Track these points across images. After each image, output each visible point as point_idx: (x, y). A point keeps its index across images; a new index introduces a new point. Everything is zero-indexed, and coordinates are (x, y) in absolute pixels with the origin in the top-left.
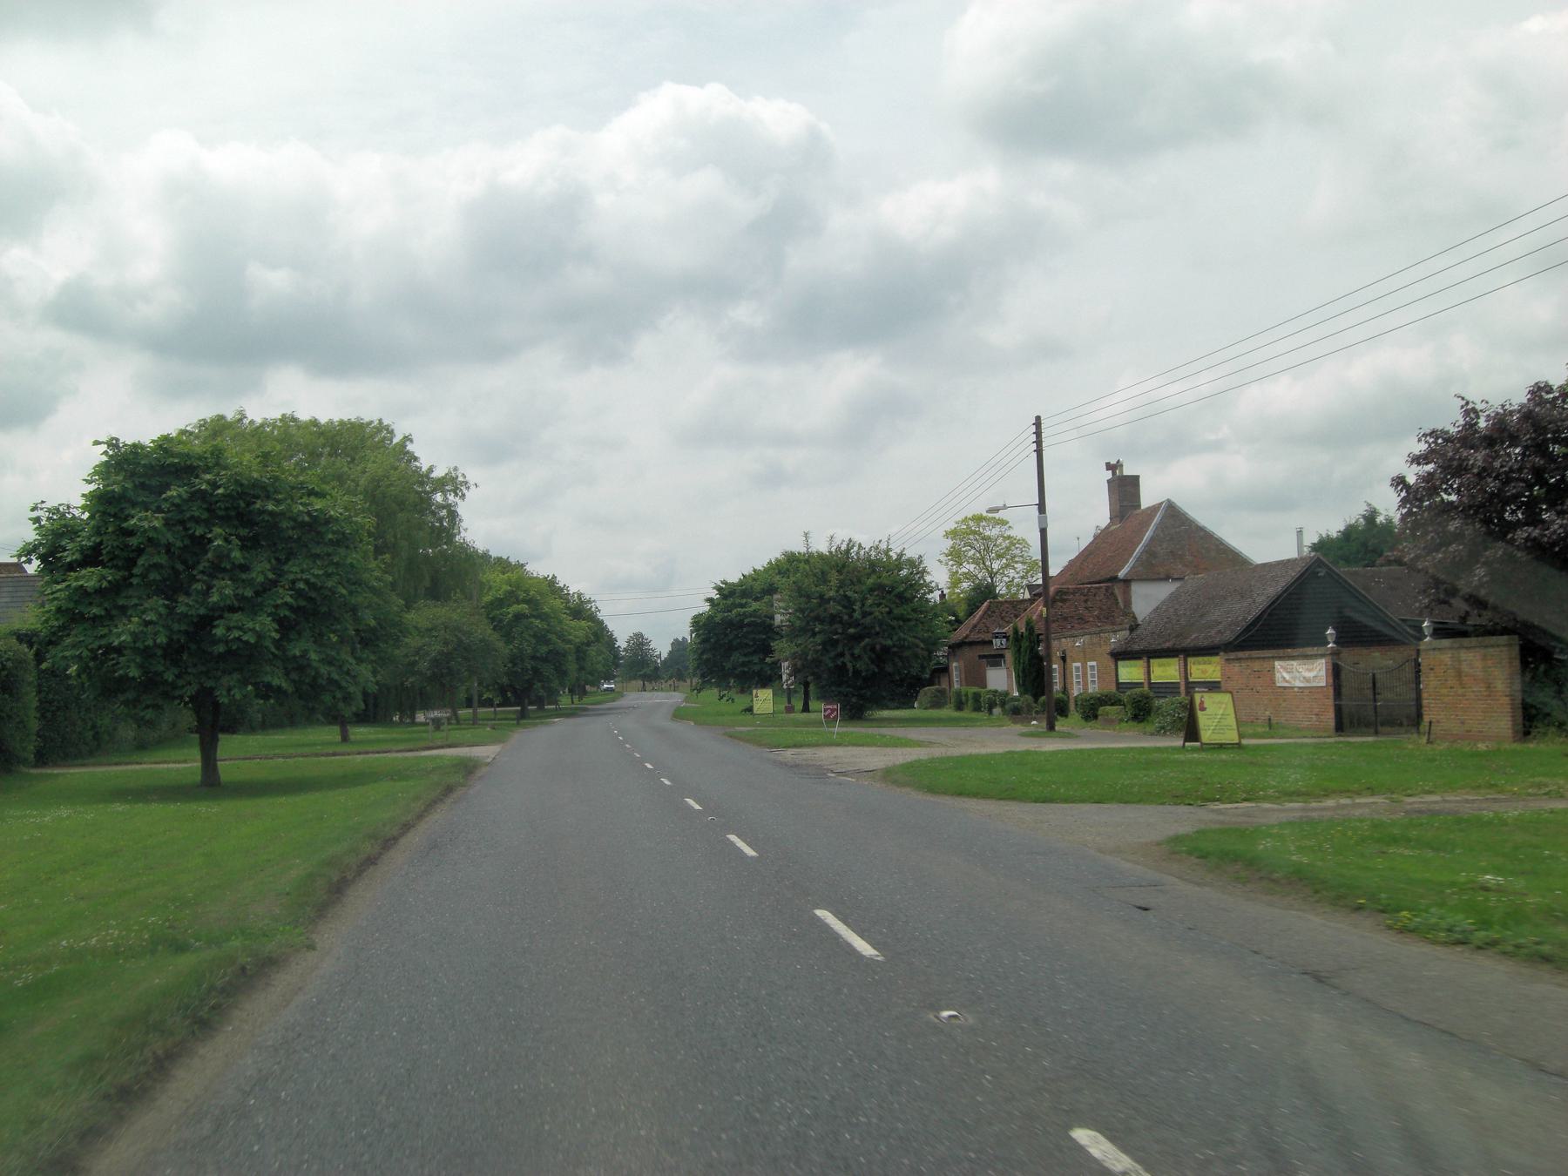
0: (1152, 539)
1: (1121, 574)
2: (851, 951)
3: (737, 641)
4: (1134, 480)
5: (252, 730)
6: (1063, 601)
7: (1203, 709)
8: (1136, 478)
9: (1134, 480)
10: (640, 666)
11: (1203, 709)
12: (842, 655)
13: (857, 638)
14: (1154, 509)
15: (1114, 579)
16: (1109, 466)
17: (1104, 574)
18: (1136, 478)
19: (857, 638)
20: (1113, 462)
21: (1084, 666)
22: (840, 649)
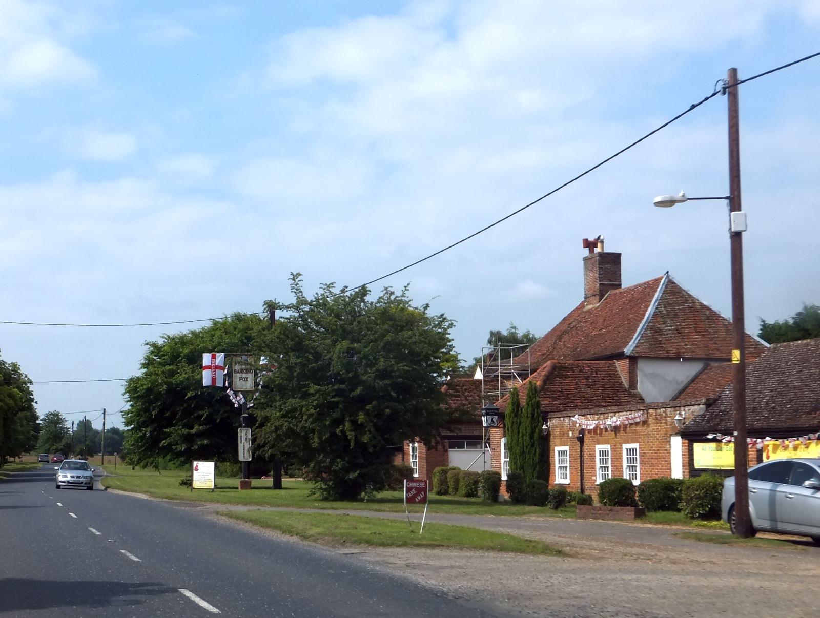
0: (655, 315)
1: (628, 350)
2: (138, 500)
3: (177, 407)
4: (615, 259)
5: (602, 444)
6: (561, 376)
7: (197, 470)
8: (618, 256)
9: (615, 259)
10: (86, 443)
11: (197, 470)
12: (339, 422)
13: (361, 401)
14: (649, 288)
15: (620, 356)
16: (590, 245)
17: (607, 347)
18: (618, 256)
19: (361, 401)
20: (591, 239)
21: (617, 452)
22: (336, 415)
